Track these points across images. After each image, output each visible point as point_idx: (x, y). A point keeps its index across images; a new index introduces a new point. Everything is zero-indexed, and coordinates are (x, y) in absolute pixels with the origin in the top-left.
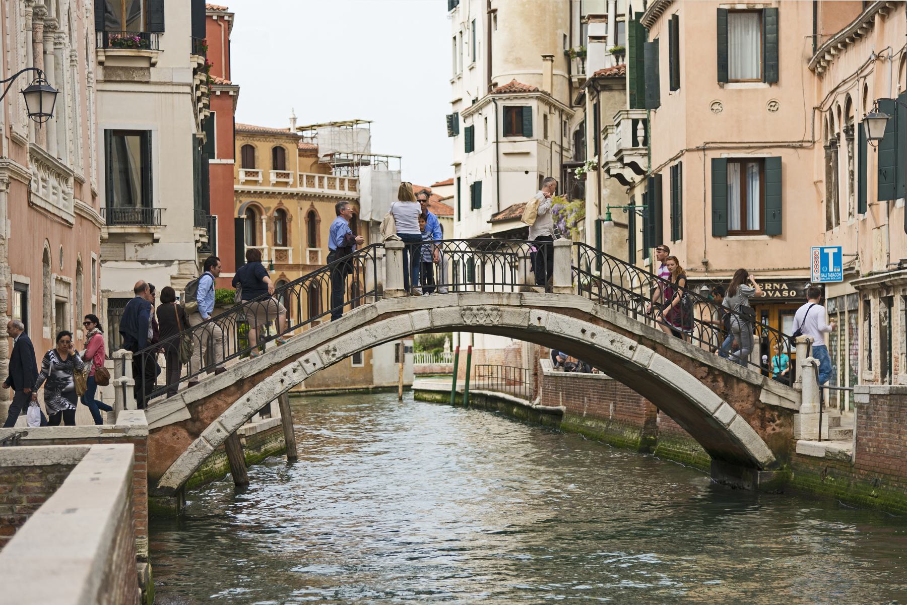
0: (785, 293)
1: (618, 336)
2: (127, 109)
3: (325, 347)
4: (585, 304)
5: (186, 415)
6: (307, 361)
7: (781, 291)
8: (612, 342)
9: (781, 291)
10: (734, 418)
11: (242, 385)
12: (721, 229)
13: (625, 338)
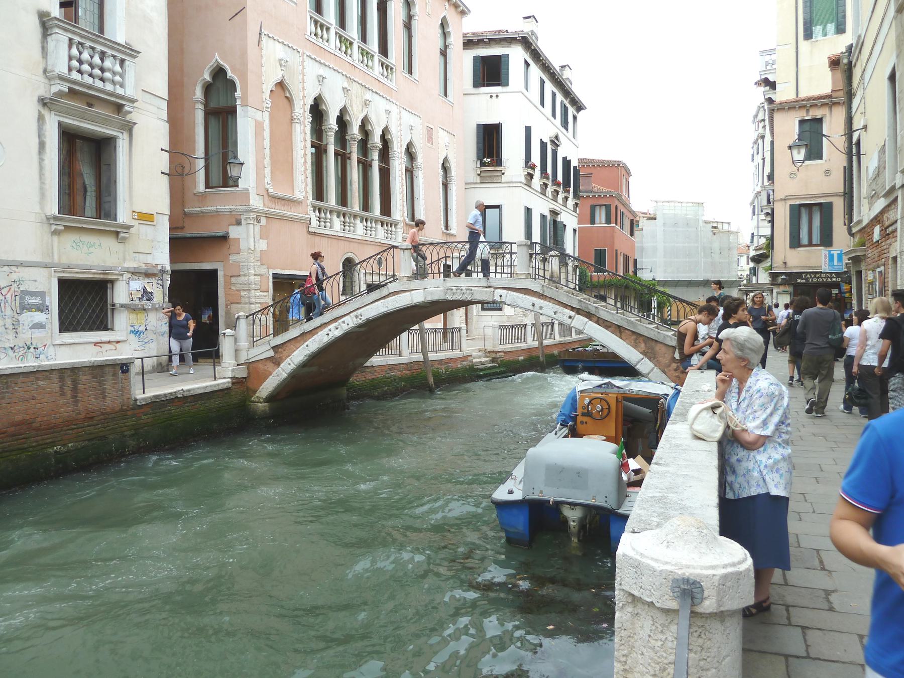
0: (834, 280)
1: (560, 309)
2: (489, 195)
3: (355, 313)
4: (535, 286)
5: (271, 353)
6: (344, 322)
7: (831, 278)
8: (555, 313)
9: (831, 278)
10: (652, 370)
11: (305, 336)
12: (795, 242)
13: (566, 310)
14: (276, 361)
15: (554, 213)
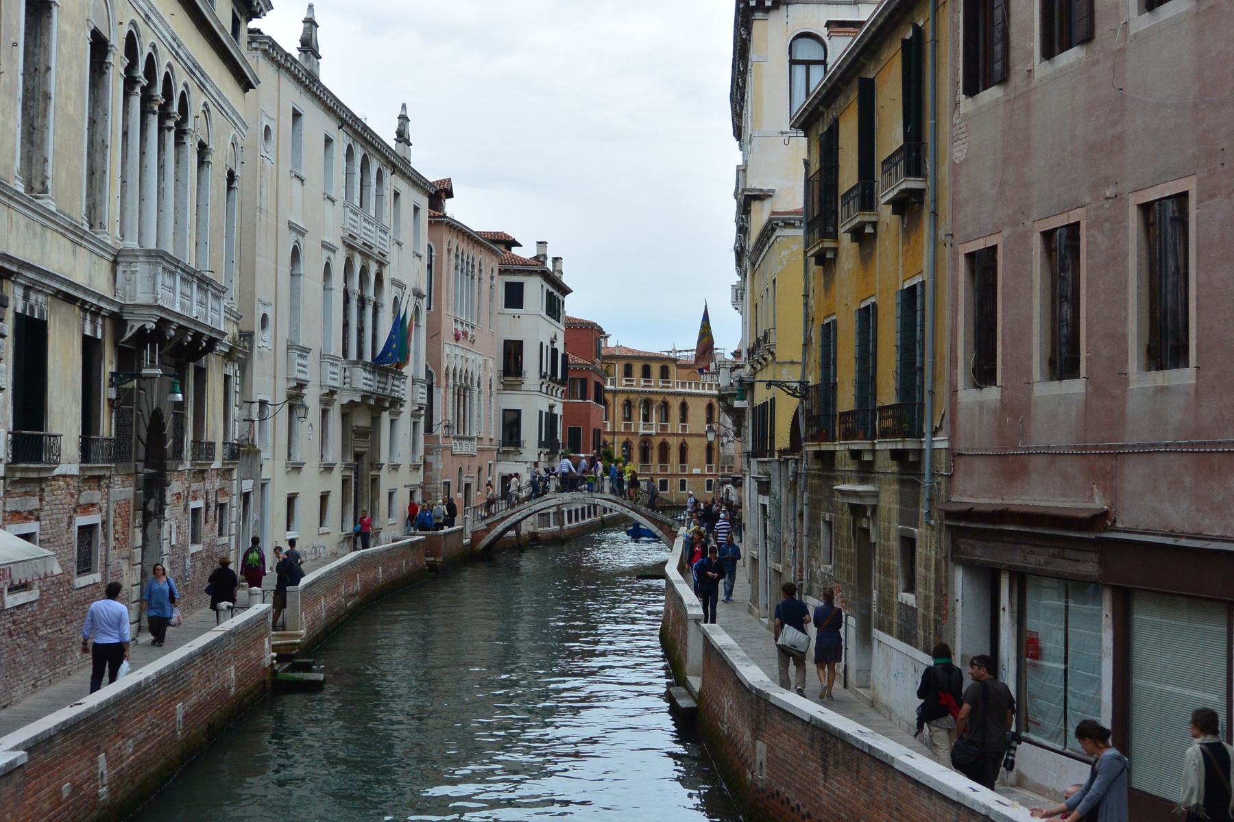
2: (512, 401)
11: (503, 519)
14: (487, 531)
15: (551, 407)
